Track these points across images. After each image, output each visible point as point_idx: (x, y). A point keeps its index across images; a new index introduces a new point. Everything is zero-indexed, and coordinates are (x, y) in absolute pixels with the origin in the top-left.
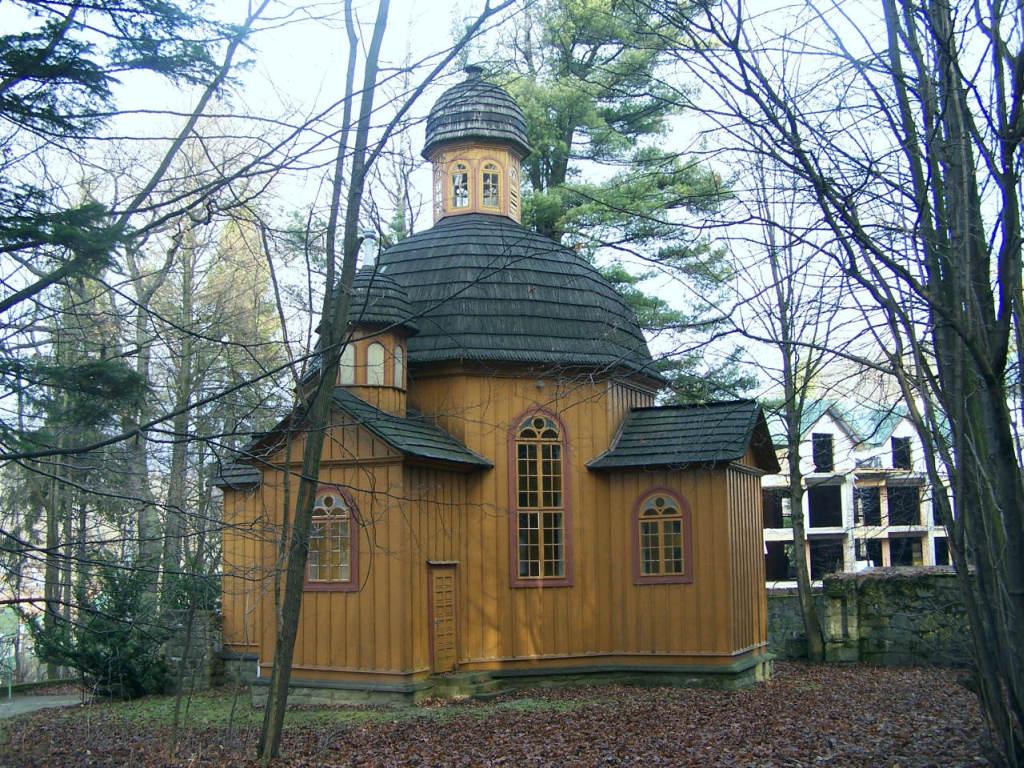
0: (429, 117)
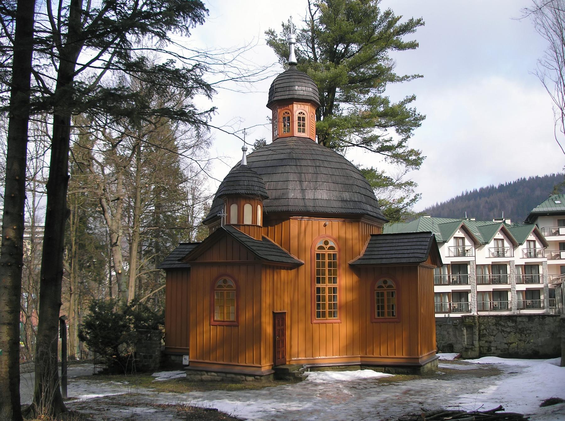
0: (216, 194)
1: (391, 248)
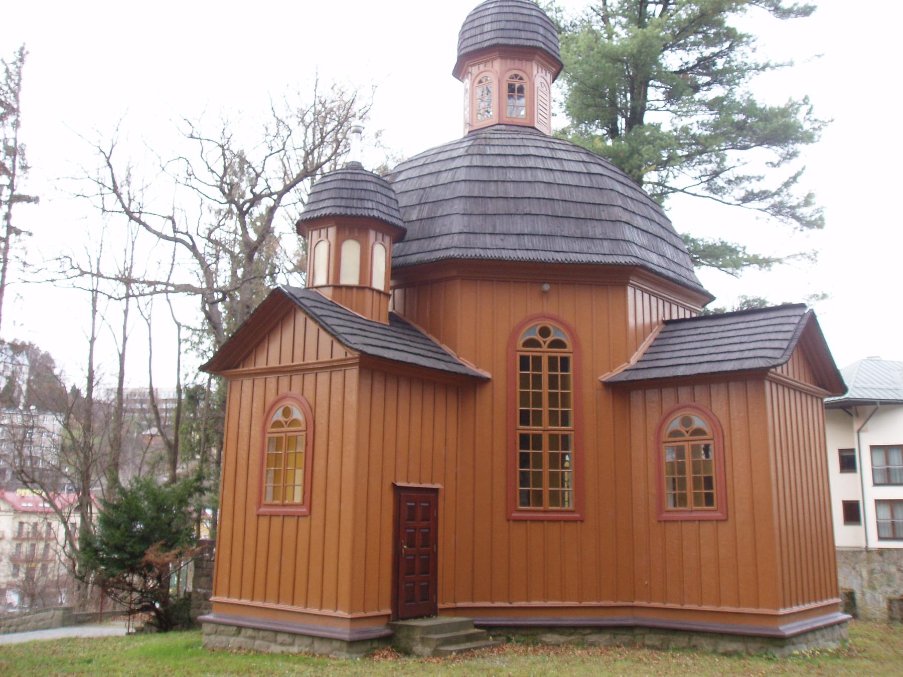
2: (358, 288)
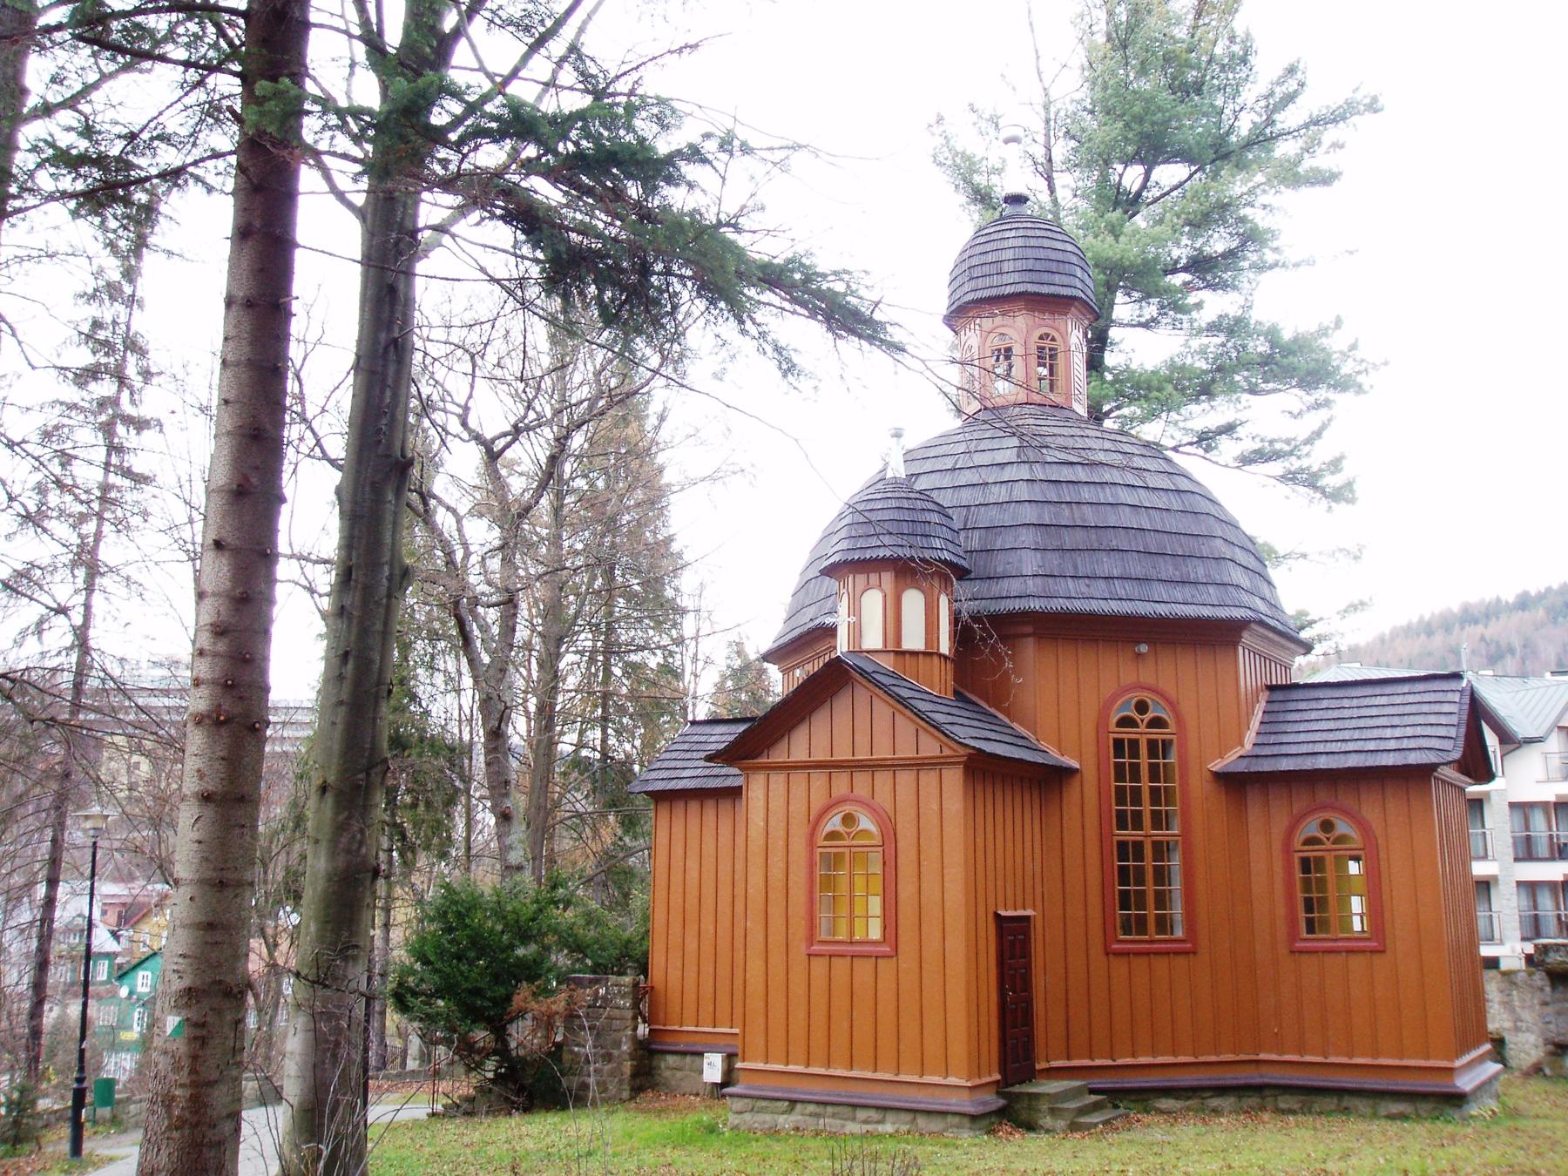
1: (1339, 724)
2: (924, 653)
